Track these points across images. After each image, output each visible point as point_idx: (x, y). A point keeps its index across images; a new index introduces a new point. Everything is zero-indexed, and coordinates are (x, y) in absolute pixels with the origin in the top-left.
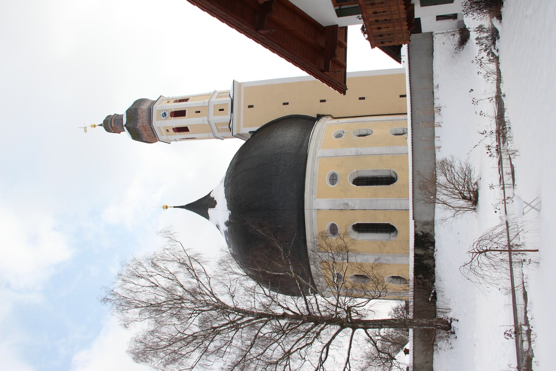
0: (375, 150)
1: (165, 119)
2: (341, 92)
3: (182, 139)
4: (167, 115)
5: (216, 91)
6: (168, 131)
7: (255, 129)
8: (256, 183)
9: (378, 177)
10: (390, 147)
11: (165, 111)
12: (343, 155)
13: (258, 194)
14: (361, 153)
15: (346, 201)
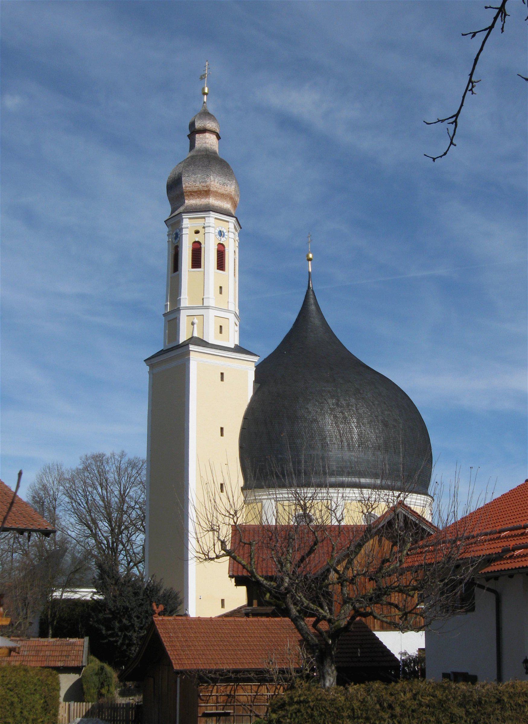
6: (197, 232)
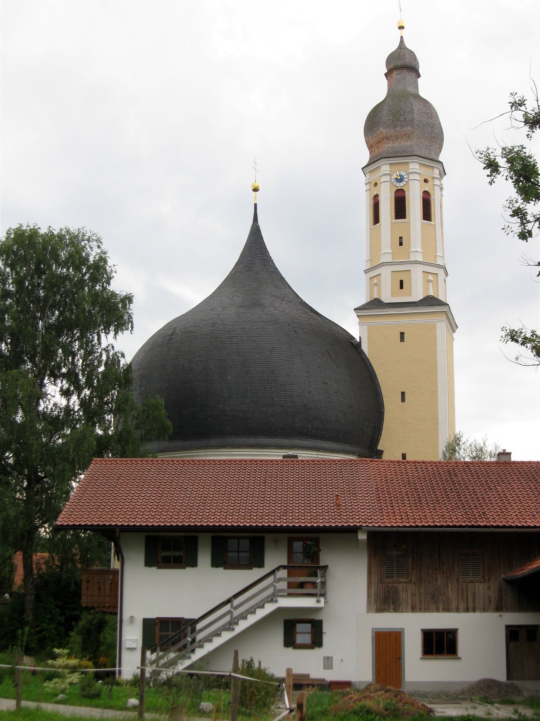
1: (392, 181)
3: (376, 197)
4: (398, 185)
7: (365, 348)
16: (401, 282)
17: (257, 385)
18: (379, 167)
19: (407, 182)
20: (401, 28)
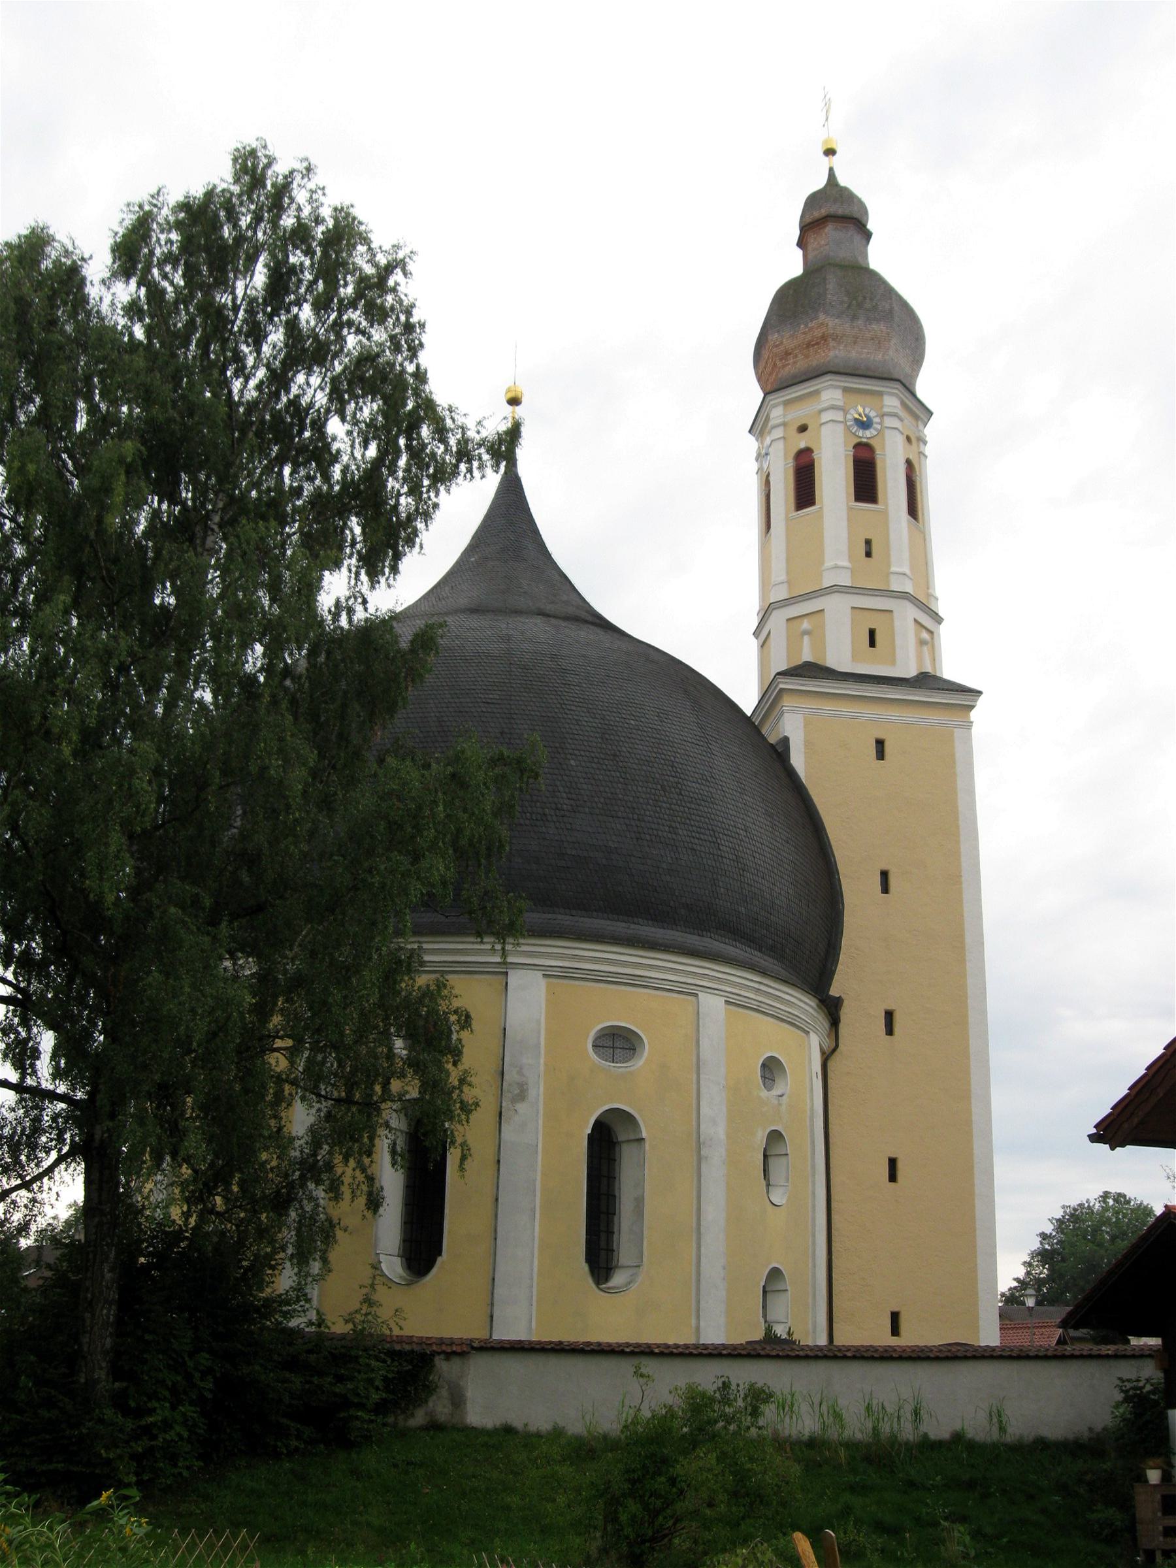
0: (714, 1212)
1: (848, 423)
2: (1102, 1127)
4: (861, 433)
5: (940, 624)
6: (803, 429)
7: (797, 760)
8: (615, 755)
9: (616, 1218)
10: (724, 1268)
11: (879, 427)
12: (703, 1090)
13: (572, 762)
14: (706, 1158)
15: (532, 1093)
16: (872, 633)
17: (640, 789)
18: (817, 393)
19: (879, 432)
20: (830, 152)
